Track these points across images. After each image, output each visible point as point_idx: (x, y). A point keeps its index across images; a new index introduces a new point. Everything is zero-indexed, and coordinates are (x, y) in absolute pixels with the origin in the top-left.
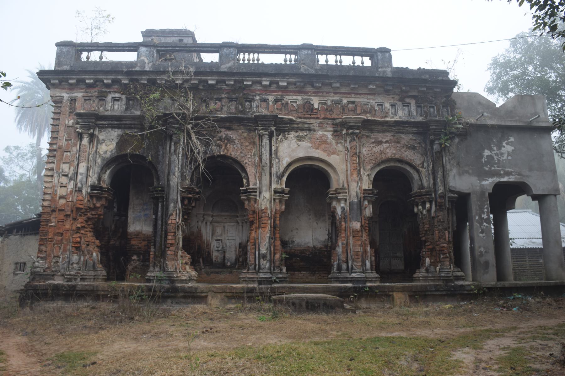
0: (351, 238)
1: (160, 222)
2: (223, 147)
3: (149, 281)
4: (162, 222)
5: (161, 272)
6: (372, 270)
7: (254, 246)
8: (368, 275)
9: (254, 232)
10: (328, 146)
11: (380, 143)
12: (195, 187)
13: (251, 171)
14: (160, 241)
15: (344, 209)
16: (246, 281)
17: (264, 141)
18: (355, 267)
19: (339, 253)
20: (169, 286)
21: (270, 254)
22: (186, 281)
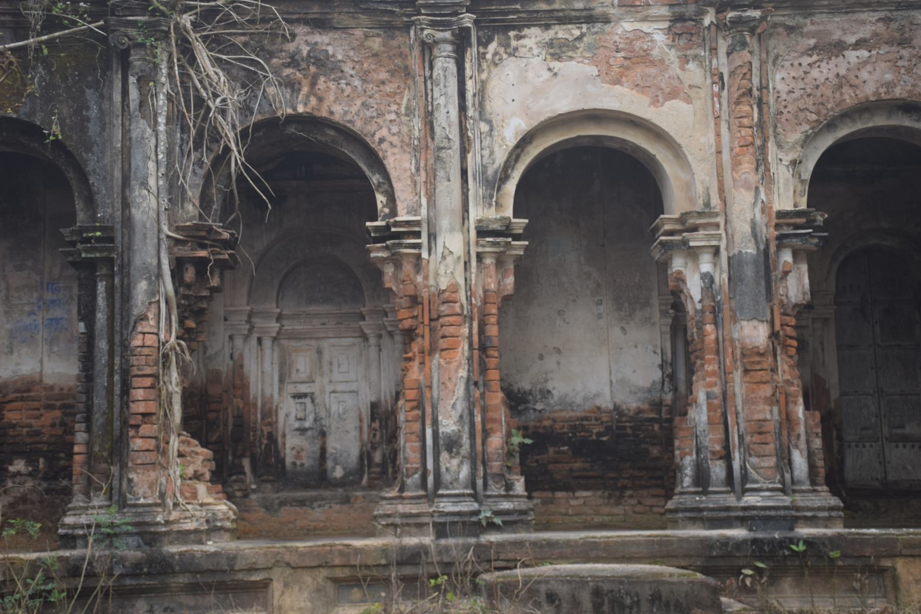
0: (737, 376)
1: (102, 345)
2: (305, 90)
3: (69, 541)
4: (111, 342)
5: (114, 509)
6: (813, 482)
7: (416, 412)
8: (800, 500)
9: (415, 365)
10: (653, 71)
11: (839, 48)
12: (216, 226)
13: (399, 164)
14: (104, 407)
15: (712, 281)
16: (395, 526)
17: (439, 64)
18: (753, 474)
19: (700, 428)
20: (139, 554)
21: (472, 436)
22: (197, 536)
